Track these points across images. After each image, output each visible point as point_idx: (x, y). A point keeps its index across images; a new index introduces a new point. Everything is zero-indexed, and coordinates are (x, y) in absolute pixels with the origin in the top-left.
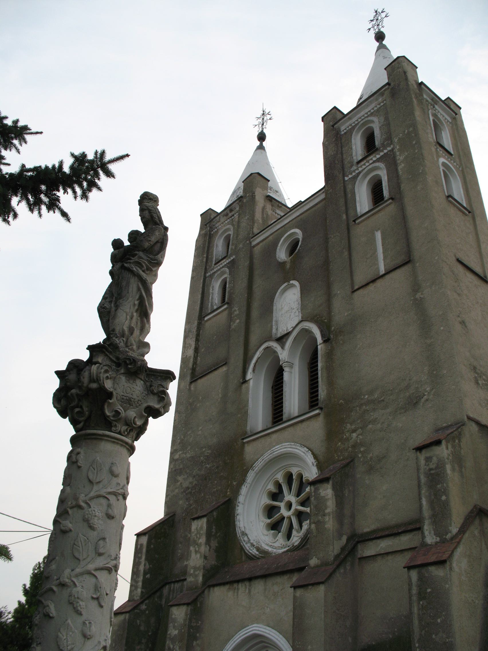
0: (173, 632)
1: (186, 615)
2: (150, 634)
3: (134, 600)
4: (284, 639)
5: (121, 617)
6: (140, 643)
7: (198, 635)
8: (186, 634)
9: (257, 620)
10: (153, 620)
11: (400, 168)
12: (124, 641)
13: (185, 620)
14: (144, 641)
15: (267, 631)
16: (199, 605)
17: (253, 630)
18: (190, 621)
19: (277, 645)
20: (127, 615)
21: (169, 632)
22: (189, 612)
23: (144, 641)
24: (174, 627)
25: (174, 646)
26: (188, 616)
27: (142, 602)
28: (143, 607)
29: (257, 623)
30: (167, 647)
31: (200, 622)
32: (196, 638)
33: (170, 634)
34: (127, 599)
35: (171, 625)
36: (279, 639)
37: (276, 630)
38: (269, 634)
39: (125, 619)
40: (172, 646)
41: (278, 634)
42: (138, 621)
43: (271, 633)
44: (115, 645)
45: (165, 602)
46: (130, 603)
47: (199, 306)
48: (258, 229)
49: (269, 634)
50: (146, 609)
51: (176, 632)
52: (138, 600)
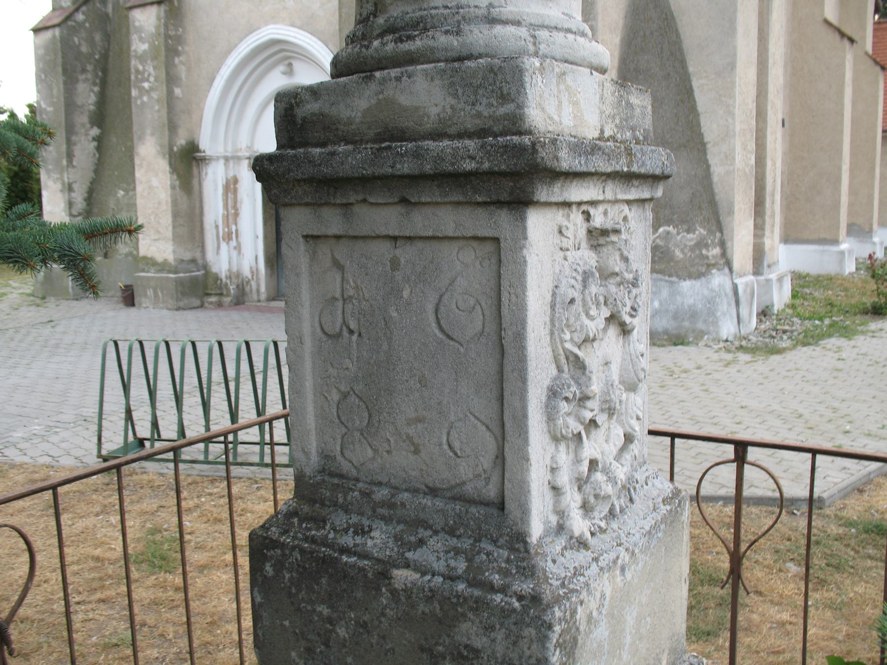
0: (139, 46)
1: (159, 19)
2: (97, 57)
3: (61, 8)
4: (320, 43)
5: (47, 35)
6: (84, 71)
7: (180, 48)
8: (163, 48)
9: (274, 19)
10: (98, 37)
11: (430, 143)
12: (60, 69)
13: (157, 28)
14: (89, 68)
15: (292, 34)
16: (176, 4)
17: (269, 34)
18: (166, 26)
19: (311, 54)
20: (57, 31)
21: (133, 48)
22: (162, 14)
23: (89, 68)
24: (141, 39)
25: (144, 67)
26: (163, 21)
27: (77, 10)
28: (80, 17)
29: (275, 23)
30: (133, 70)
31: (180, 30)
32: (177, 53)
33: (135, 51)
34: (51, 9)
35: (134, 37)
36: (312, 43)
37: (305, 30)
38: (295, 38)
39: (54, 36)
40: (141, 68)
41: (309, 36)
42: (76, 39)
43: (298, 36)
44: (46, 76)
45: (113, 9)
46: (57, 13)
47: (768, 150)
48: (797, 478)
49: (295, 38)
50: (85, 21)
51: (145, 47)
52: (69, 7)
